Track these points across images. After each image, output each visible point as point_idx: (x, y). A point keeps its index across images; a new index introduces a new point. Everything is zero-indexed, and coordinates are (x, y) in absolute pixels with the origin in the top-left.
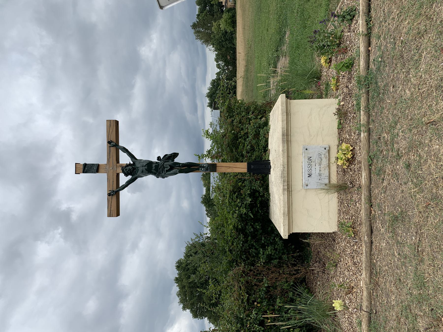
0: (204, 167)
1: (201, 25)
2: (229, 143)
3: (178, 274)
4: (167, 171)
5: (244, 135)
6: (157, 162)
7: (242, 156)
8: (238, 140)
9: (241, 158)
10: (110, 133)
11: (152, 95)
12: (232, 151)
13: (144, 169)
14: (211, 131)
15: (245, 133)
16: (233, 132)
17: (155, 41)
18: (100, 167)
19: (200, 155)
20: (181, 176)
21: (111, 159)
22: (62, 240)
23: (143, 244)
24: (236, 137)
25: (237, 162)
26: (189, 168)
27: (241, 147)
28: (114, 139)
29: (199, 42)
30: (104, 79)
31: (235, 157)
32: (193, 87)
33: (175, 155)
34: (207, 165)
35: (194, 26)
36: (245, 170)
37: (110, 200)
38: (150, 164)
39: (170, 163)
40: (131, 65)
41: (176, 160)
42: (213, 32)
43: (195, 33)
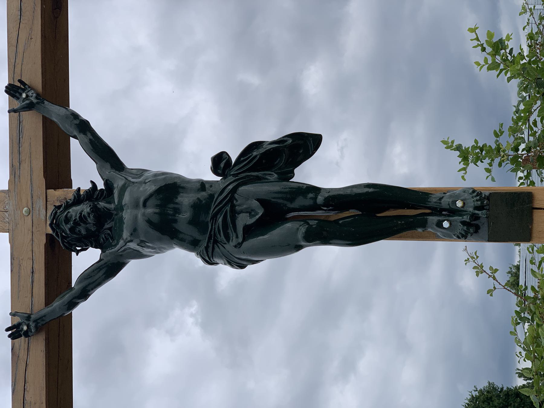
0: (453, 212)
4: (250, 231)
6: (203, 185)
21: (25, 166)
22: (196, 331)
23: (368, 362)
26: (375, 214)
28: (34, 77)
33: (304, 145)
34: (472, 203)
37: (23, 354)
38: (170, 189)
39: (270, 188)
41: (312, 173)
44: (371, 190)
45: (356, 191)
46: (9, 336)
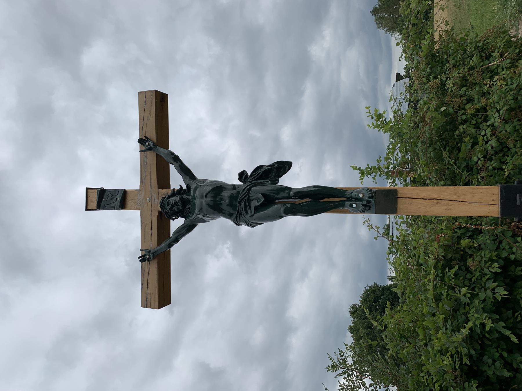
0: (358, 199)
1: (384, 8)
2: (431, 139)
3: (353, 322)
4: (257, 209)
5: (474, 115)
6: (234, 187)
7: (469, 168)
8: (457, 128)
9: (465, 174)
10: (145, 121)
11: (323, 102)
12: (440, 158)
13: (204, 203)
14: (390, 116)
15: (478, 110)
16: (443, 109)
17: (327, 38)
18: (129, 197)
19: (363, 168)
20: (294, 223)
21: (148, 178)
23: (314, 272)
24: (452, 122)
25: (454, 183)
26: (318, 200)
27: (466, 146)
28: (152, 134)
29: (382, 32)
30: (271, 87)
31: (447, 172)
32: (374, 89)
33: (283, 167)
35: (375, 11)
36: (494, 211)
37: (146, 270)
38: (218, 188)
39: (267, 188)
40: (300, 68)
41: (285, 181)
42: (400, 16)
43: (376, 20)
44: (317, 189)
45: (309, 189)
46: (140, 261)
